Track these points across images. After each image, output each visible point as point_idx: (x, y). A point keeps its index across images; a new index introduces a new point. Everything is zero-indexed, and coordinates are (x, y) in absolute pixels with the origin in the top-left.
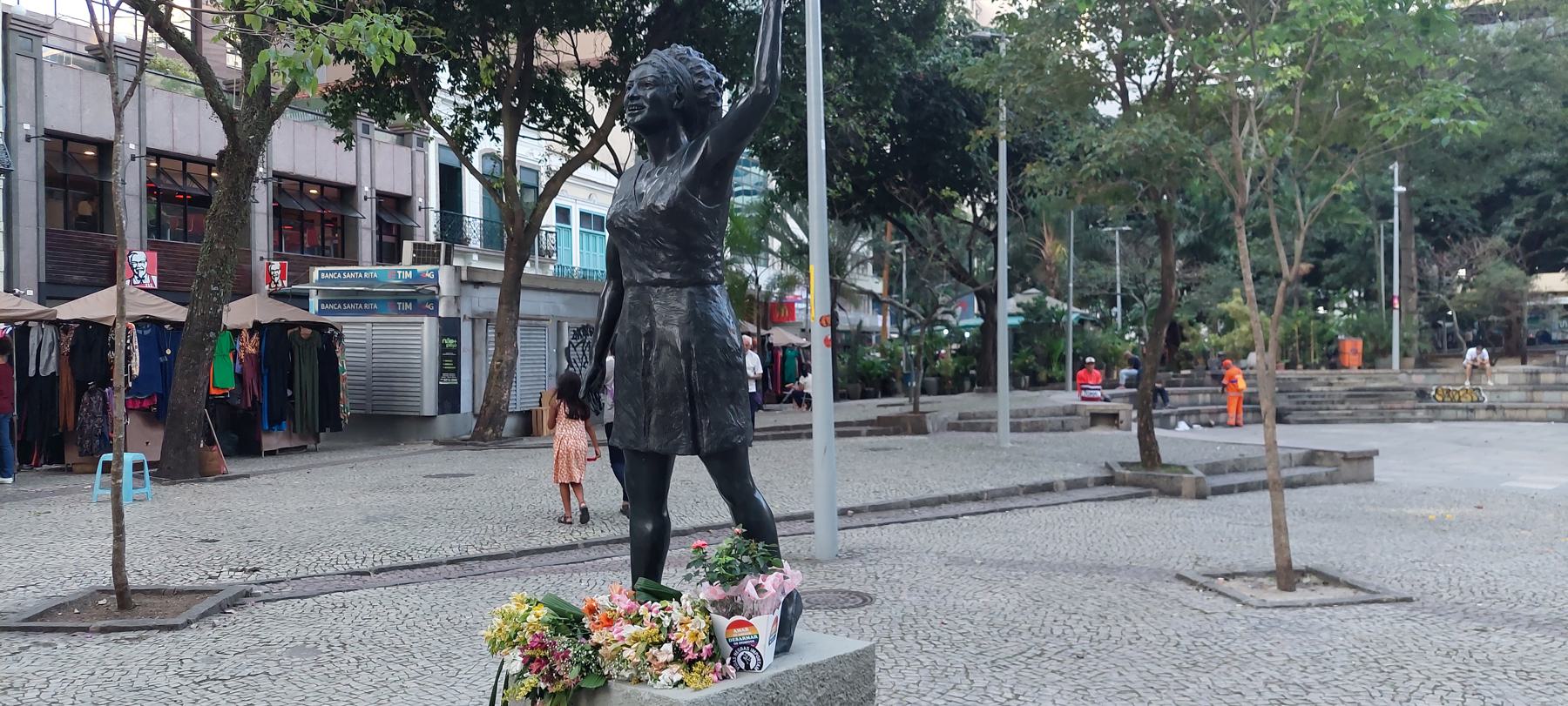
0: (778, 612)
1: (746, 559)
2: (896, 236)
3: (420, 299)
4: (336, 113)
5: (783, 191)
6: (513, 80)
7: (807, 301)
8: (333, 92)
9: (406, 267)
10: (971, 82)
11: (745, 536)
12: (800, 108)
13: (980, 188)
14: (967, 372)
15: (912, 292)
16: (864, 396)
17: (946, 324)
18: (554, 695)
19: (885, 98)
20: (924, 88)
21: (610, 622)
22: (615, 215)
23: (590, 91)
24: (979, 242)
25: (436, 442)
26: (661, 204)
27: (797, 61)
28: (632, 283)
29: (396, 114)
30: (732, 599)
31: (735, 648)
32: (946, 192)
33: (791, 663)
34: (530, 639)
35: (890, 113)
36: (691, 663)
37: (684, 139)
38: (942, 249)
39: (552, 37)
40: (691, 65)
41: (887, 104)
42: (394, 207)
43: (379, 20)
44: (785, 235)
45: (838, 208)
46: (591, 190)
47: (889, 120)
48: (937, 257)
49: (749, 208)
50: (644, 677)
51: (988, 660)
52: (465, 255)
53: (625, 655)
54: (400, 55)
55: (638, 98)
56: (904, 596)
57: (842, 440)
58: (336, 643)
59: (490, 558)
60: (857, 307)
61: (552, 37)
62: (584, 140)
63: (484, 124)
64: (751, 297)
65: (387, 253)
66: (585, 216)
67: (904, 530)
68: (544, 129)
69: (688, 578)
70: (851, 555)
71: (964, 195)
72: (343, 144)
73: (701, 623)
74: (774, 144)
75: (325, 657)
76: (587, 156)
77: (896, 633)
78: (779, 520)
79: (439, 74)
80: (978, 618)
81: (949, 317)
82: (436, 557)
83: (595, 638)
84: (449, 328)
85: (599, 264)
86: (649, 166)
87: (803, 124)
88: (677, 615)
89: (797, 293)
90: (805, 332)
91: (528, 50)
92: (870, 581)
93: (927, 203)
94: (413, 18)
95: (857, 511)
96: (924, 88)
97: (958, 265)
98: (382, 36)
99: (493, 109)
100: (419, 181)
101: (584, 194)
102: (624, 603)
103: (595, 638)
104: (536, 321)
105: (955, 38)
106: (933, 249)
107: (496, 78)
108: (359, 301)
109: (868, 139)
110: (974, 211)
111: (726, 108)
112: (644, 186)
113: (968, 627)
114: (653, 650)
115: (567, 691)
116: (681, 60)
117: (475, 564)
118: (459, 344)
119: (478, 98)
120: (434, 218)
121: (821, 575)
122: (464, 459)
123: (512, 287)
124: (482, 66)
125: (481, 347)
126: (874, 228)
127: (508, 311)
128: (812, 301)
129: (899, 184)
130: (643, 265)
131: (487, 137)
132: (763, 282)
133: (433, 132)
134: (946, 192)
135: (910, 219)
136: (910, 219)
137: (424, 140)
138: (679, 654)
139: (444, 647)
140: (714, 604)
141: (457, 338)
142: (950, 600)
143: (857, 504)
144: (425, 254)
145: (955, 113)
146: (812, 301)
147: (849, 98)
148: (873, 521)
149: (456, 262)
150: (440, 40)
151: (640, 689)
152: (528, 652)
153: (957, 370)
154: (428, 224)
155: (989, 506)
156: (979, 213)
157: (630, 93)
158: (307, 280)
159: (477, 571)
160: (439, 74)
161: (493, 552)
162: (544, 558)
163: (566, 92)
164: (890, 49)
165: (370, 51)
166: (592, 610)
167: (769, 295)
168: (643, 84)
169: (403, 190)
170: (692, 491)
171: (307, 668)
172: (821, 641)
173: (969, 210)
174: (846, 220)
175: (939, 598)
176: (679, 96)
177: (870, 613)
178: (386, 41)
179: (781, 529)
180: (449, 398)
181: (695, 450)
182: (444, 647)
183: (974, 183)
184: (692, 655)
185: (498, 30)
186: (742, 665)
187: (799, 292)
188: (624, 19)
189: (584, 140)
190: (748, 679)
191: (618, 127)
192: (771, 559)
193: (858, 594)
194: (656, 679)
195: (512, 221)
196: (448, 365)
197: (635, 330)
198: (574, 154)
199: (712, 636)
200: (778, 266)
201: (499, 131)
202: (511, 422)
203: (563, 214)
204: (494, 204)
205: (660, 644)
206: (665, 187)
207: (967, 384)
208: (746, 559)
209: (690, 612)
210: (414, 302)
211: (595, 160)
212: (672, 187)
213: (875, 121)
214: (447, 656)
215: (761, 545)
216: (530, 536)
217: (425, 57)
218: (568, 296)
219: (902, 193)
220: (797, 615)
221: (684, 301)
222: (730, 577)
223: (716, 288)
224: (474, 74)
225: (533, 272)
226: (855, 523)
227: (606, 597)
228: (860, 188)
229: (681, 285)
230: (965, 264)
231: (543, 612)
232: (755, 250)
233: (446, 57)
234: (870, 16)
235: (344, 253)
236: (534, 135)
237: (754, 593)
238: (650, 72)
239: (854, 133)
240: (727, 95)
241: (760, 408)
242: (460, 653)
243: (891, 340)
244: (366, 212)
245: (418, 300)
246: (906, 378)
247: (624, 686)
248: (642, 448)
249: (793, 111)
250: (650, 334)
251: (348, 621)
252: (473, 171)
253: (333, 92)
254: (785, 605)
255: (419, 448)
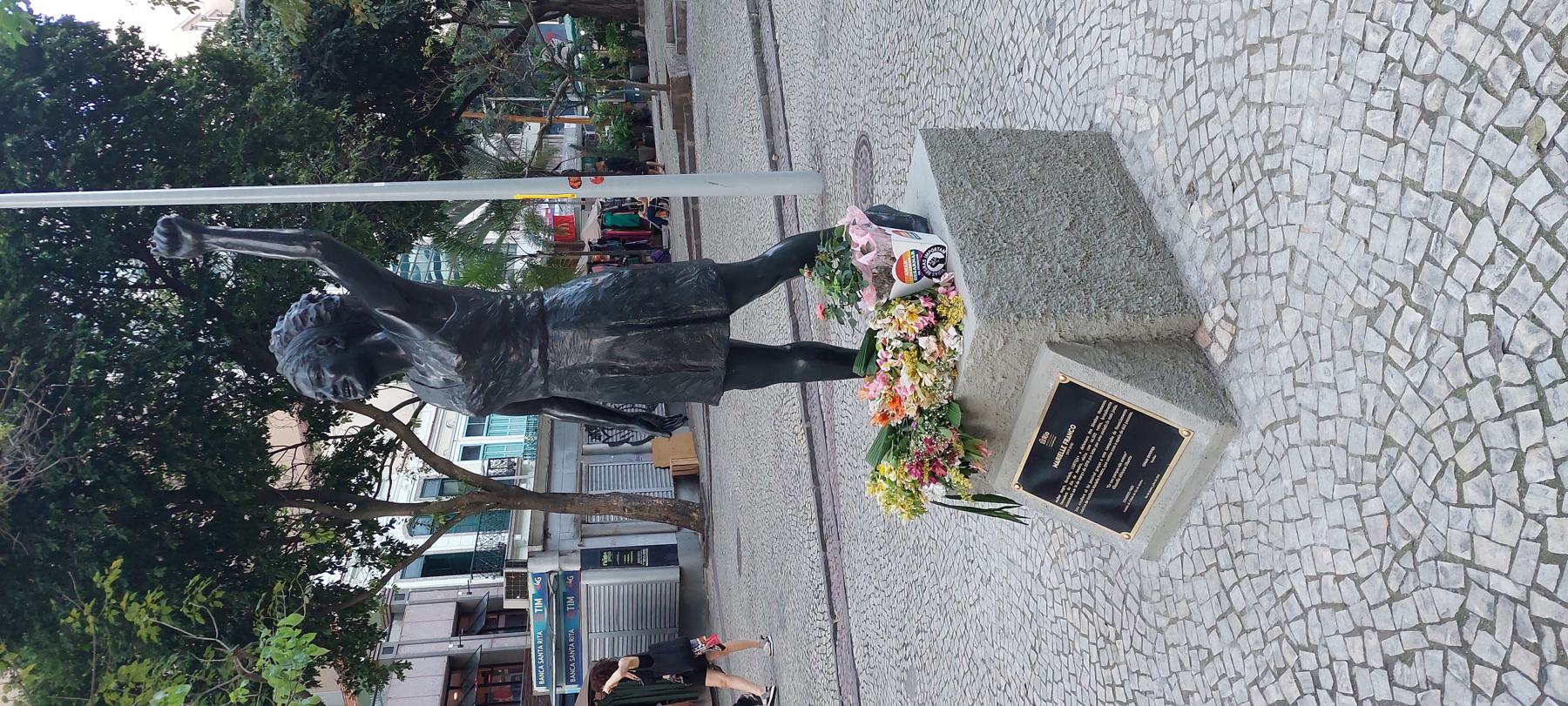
0: (889, 230)
1: (835, 264)
2: (477, 108)
3: (563, 589)
4: (372, 681)
5: (435, 229)
6: (327, 510)
7: (551, 203)
8: (349, 686)
9: (531, 604)
10: (299, 21)
11: (811, 266)
12: (341, 210)
13: (420, 14)
14: (624, 34)
15: (540, 94)
16: (651, 143)
17: (570, 57)
18: (967, 452)
19: (324, 117)
20: (310, 74)
21: (896, 400)
22: (470, 408)
23: (335, 431)
24: (481, 17)
25: (705, 566)
26: (455, 360)
27: (288, 213)
28: (545, 388)
29: (370, 623)
30: (875, 277)
31: (924, 274)
32: (427, 51)
33: (938, 217)
34: (912, 477)
35: (341, 113)
36: (938, 318)
37: (379, 336)
38: (490, 57)
39: (277, 472)
40: (293, 330)
41: (331, 115)
42: (468, 618)
43: (267, 653)
44: (481, 226)
45: (450, 170)
46: (437, 427)
47: (349, 114)
48: (499, 63)
49: (453, 265)
50: (952, 364)
51: (926, 13)
52: (516, 547)
53: (929, 384)
54: (305, 628)
55: (335, 387)
56: (860, 102)
57: (699, 167)
58: (903, 653)
59: (820, 511)
60: (557, 150)
61: (277, 472)
62: (389, 435)
63: (376, 536)
64: (550, 262)
65: (518, 621)
66: (470, 432)
67: (792, 103)
68: (379, 476)
69: (853, 323)
70: (817, 157)
71: (429, 33)
72: (405, 672)
73: (899, 309)
74: (382, 238)
75: (917, 663)
76: (406, 432)
77: (899, 110)
78: (783, 233)
79: (325, 583)
80: (882, 23)
81: (564, 51)
82: (819, 562)
83: (912, 413)
84: (591, 559)
85: (522, 420)
86: (412, 372)
87: (359, 206)
88: (891, 333)
89: (543, 214)
90: (585, 204)
91: (293, 496)
92: (845, 138)
93: (440, 72)
94: (265, 613)
95: (772, 152)
96: (310, 74)
97: (507, 40)
98: (283, 646)
99: (360, 528)
100: (441, 596)
101: (447, 433)
102: (878, 386)
103: (912, 413)
104: (582, 476)
105: (250, 39)
106: (491, 67)
107: (325, 527)
108: (567, 647)
109: (371, 138)
110: (447, 21)
111: (343, 291)
112: (435, 378)
113: (892, 34)
114: (926, 356)
115: (963, 439)
116: (288, 342)
117: (826, 525)
118: (607, 550)
119: (349, 543)
120: (479, 579)
121: (838, 188)
122: (723, 537)
123: (548, 501)
124: (314, 541)
125: (610, 529)
126: (471, 131)
127: (572, 504)
128: (552, 196)
129: (420, 104)
130: (524, 378)
131: (391, 532)
132: (533, 250)
133: (388, 586)
134: (427, 51)
135: (458, 93)
136: (458, 93)
137: (398, 594)
138: (929, 331)
139: (908, 552)
140: (880, 296)
141: (602, 551)
142: (864, 53)
143: (766, 152)
144: (517, 587)
145: (337, 40)
146: (552, 196)
147: (326, 157)
148: (782, 134)
149: (524, 556)
150: (288, 585)
151: (963, 367)
152: (926, 480)
153: (619, 44)
154: (486, 585)
155: (765, 12)
156: (448, 16)
157: (330, 396)
158: (546, 698)
159: (833, 523)
160: (325, 583)
161: (814, 508)
162: (821, 460)
163: (337, 456)
164: (267, 112)
165: (302, 659)
166: (885, 416)
167: (546, 243)
168: (319, 382)
169: (450, 611)
170: (762, 321)
171: (926, 679)
172: (916, 183)
173: (446, 28)
174: (462, 162)
175: (861, 64)
176: (330, 342)
177: (878, 137)
178: (290, 644)
179: (792, 231)
180: (662, 556)
181: (725, 319)
182: (908, 552)
183: (415, 20)
184: (931, 317)
185: (273, 526)
186: (941, 266)
187: (542, 211)
188: (252, 398)
189: (389, 435)
190: (955, 260)
191: (372, 401)
192: (836, 238)
193: (857, 150)
194: (954, 352)
195: (479, 504)
196: (629, 558)
197: (596, 384)
198: (404, 445)
199: (911, 297)
200: (516, 234)
201: (383, 521)
202: (686, 495)
203: (469, 453)
204: (466, 521)
205: (919, 350)
206: (435, 356)
207: (635, 33)
208: (835, 264)
209: (888, 320)
210: (565, 595)
211: (410, 424)
212: (436, 348)
213: (350, 129)
214: (916, 550)
215: (820, 249)
216: (798, 473)
217: (306, 600)
218: (556, 446)
219: (431, 100)
220: (890, 211)
221: (563, 333)
222: (853, 281)
223: (547, 300)
224: (321, 549)
225: (532, 481)
226: (785, 154)
227: (871, 404)
228: (428, 146)
229: (546, 337)
230: (505, 33)
231: (886, 466)
232: (498, 259)
233: (305, 578)
234: (232, 133)
235: (519, 663)
236: (386, 485)
237: (870, 256)
238: (303, 375)
239: (365, 152)
240: (331, 289)
241: (667, 252)
242: (913, 537)
243: (590, 114)
244: (474, 644)
245: (564, 591)
246: (631, 99)
247: (959, 384)
248: (722, 374)
249: (344, 218)
250: (601, 368)
251: (881, 642)
252: (428, 544)
253: (349, 686)
254: (880, 223)
255: (711, 581)
